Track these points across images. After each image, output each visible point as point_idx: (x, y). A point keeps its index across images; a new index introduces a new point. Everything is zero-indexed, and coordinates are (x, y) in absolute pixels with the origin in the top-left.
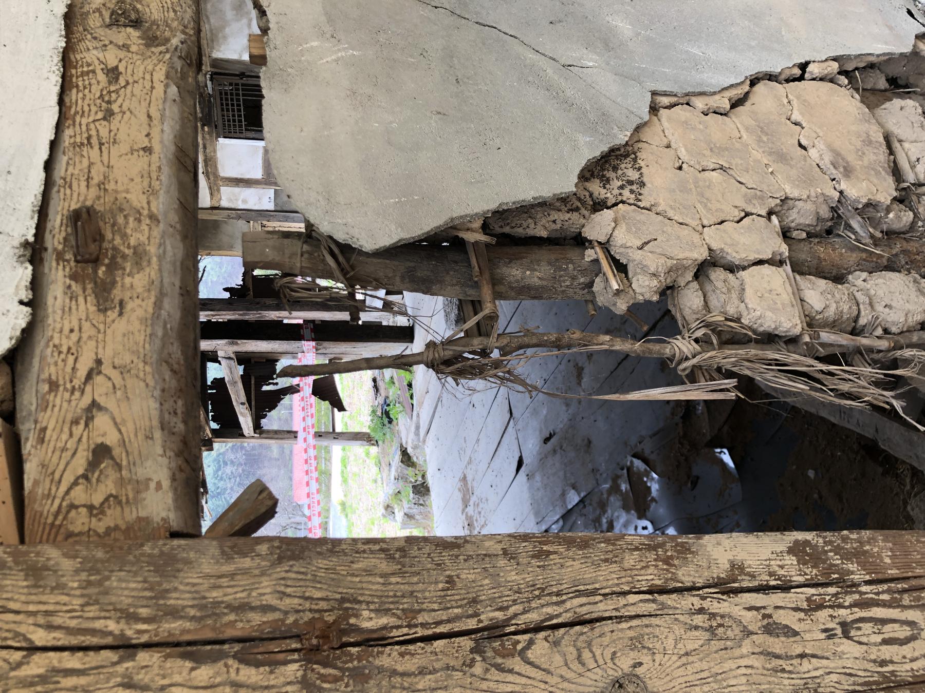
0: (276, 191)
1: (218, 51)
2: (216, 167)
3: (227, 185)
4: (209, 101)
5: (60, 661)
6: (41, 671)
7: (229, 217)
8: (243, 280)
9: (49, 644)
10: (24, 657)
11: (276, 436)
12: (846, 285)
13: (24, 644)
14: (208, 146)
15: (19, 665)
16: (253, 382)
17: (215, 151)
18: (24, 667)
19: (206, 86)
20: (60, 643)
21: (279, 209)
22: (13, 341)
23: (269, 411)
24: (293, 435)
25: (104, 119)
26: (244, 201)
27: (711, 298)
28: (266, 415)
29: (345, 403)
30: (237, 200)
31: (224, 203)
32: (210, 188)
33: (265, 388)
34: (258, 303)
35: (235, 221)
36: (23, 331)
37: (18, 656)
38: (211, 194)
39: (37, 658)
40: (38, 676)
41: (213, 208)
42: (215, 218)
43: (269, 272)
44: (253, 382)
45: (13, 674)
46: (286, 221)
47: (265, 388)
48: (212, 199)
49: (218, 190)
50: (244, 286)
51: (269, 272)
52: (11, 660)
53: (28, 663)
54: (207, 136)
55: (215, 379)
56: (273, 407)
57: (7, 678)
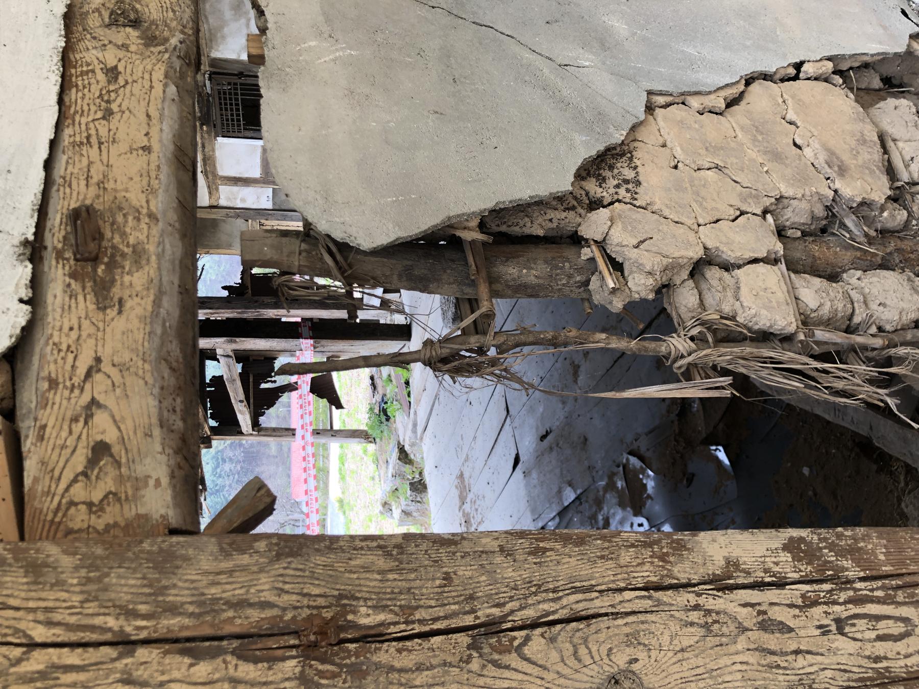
0: (274, 190)
1: (217, 50)
2: (214, 166)
3: (226, 184)
4: (208, 101)
5: (59, 658)
6: (41, 667)
7: (227, 216)
8: (241, 278)
9: (49, 640)
10: (24, 653)
11: (274, 434)
12: (840, 283)
13: (24, 641)
14: (206, 145)
15: (19, 661)
16: (251, 380)
17: (213, 150)
18: (24, 663)
19: (205, 86)
20: (59, 640)
21: (277, 207)
22: (13, 340)
23: (268, 409)
24: (291, 433)
25: (104, 118)
26: (243, 200)
27: (706, 296)
28: (264, 413)
29: (343, 401)
30: (235, 199)
31: (223, 202)
32: (209, 187)
33: (263, 386)
34: (256, 302)
35: (233, 220)
36: (23, 329)
37: (18, 652)
38: (210, 193)
39: (37, 654)
40: (38, 672)
41: (212, 207)
42: (213, 216)
43: (267, 271)
44: (251, 380)
45: (12, 670)
46: (285, 220)
47: (263, 386)
48: (210, 198)
49: (217, 189)
50: (242, 284)
51: (267, 271)
52: (11, 657)
53: (28, 659)
54: (206, 136)
55: (214, 377)
56: (271, 404)
57: (7, 674)
